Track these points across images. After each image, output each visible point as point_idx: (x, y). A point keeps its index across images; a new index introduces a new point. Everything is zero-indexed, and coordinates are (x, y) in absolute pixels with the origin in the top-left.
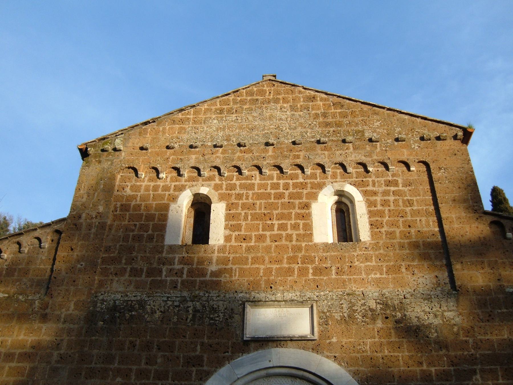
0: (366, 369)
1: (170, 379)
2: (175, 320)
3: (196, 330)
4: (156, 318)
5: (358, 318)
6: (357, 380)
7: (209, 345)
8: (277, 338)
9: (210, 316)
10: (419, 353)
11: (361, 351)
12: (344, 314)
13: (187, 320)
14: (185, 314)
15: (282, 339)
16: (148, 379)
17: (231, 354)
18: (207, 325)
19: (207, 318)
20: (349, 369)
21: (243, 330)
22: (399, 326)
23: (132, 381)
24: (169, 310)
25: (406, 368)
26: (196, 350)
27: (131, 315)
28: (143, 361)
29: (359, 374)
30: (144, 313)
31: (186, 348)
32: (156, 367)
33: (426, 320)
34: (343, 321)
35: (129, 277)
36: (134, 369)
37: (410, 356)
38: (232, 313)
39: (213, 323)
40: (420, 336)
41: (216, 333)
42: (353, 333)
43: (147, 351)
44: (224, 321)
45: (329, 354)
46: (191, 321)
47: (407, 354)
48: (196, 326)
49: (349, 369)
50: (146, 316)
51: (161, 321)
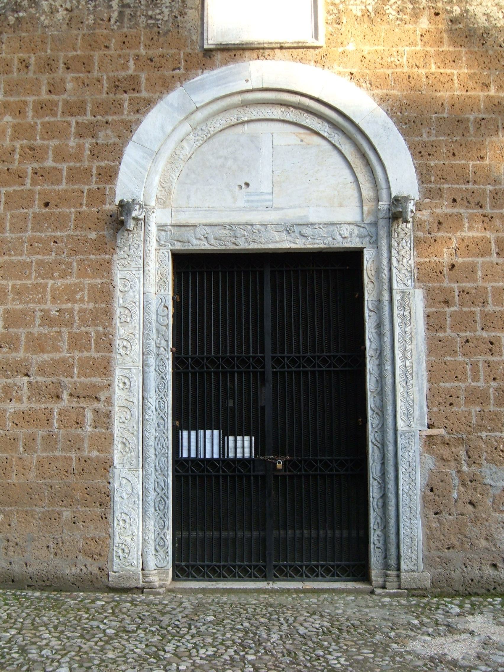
0: (400, 93)
1: (89, 113)
2: (91, 22)
3: (126, 37)
4: (59, 20)
5: (390, 13)
6: (385, 108)
7: (148, 59)
8: (259, 44)
9: (147, 13)
10: (485, 70)
11: (393, 66)
12: (368, 7)
13: (109, 20)
14: (106, 11)
15: (266, 46)
16: (55, 115)
17: (184, 72)
18: (144, 28)
19: (143, 17)
20: (373, 92)
21: (202, 34)
22: (457, 27)
23: (29, 119)
24: (79, 6)
25: (464, 93)
26: (128, 68)
27: (17, 18)
28: (44, 89)
29: (388, 100)
30: (39, 12)
31: (111, 65)
32: (65, 96)
33: (500, 19)
34: (366, 18)
35: (48, 94)
36: (30, 102)
37: (470, 74)
38: (183, 7)
39: (153, 24)
40: (488, 43)
41: (159, 40)
42: (382, 38)
43: (48, 72)
44: (171, 20)
45: (341, 69)
46: (116, 22)
47: (466, 71)
48: (125, 30)
49: (373, 92)
50: (43, 18)
51: (68, 24)
